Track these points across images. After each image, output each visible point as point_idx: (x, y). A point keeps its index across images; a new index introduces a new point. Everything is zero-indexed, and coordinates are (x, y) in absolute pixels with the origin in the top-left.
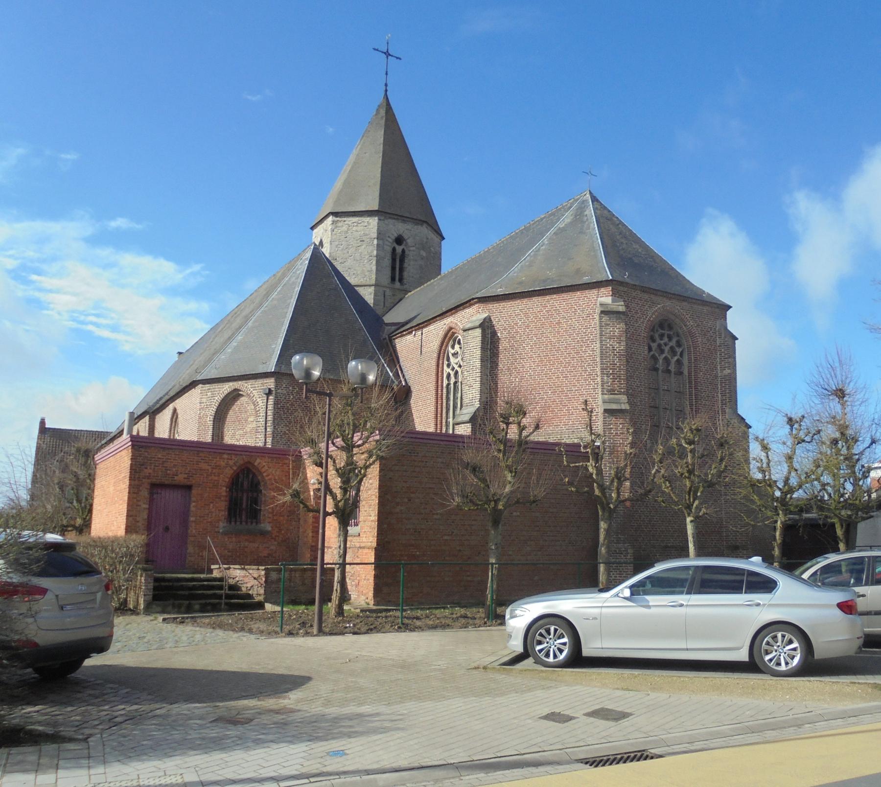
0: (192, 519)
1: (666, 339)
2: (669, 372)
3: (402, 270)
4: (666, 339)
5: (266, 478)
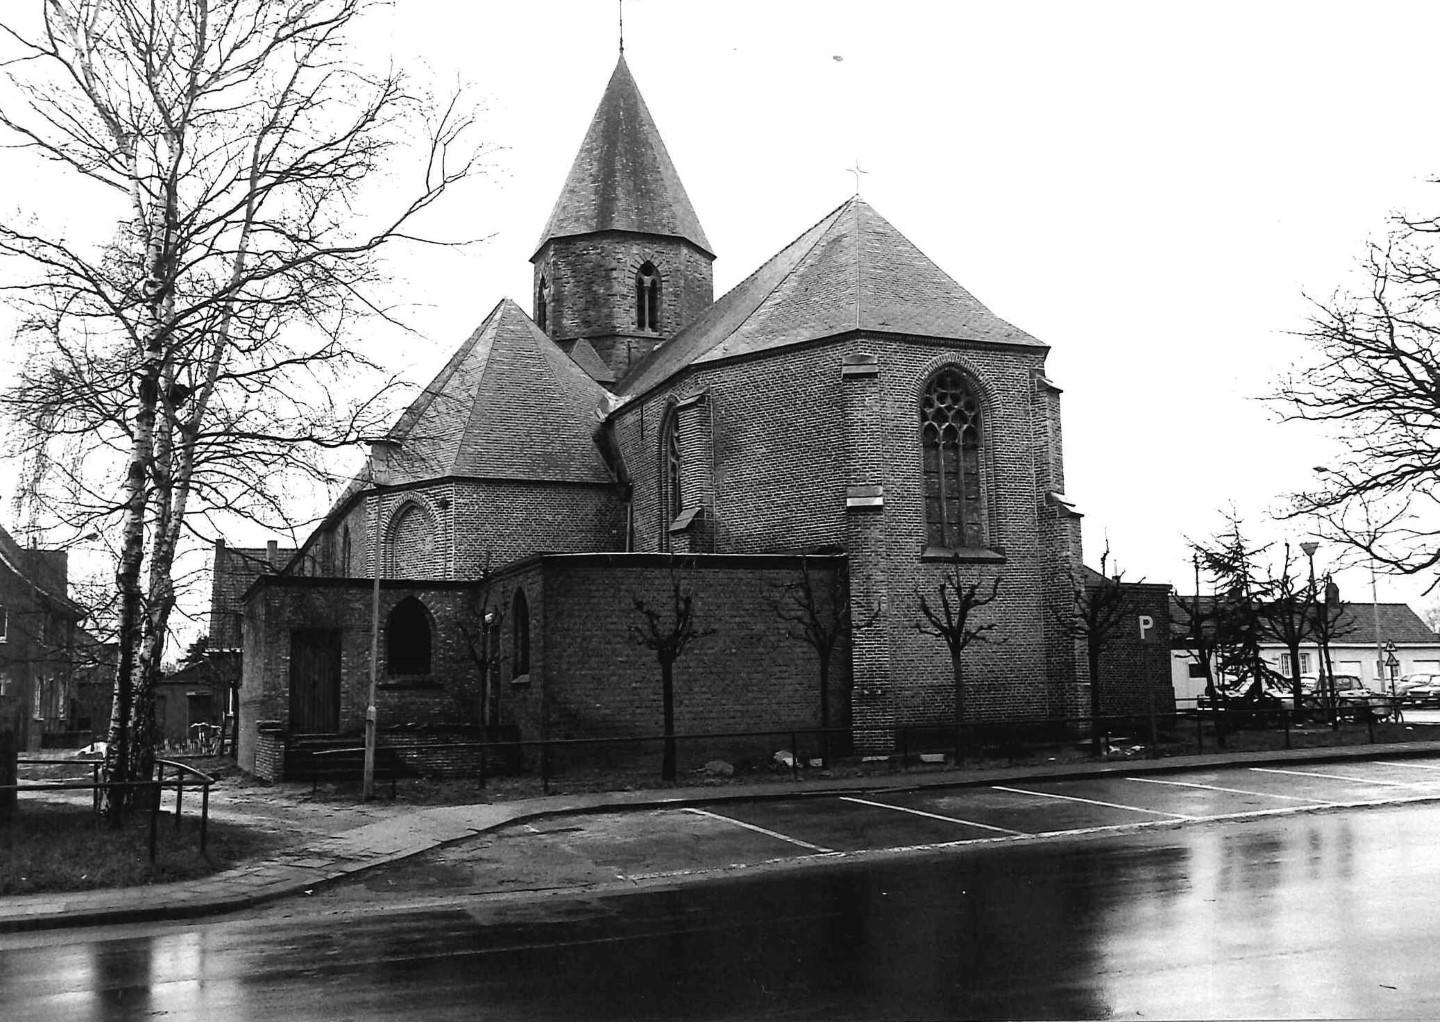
0: (343, 671)
1: (949, 401)
2: (955, 447)
3: (653, 309)
4: (949, 401)
5: (435, 616)
